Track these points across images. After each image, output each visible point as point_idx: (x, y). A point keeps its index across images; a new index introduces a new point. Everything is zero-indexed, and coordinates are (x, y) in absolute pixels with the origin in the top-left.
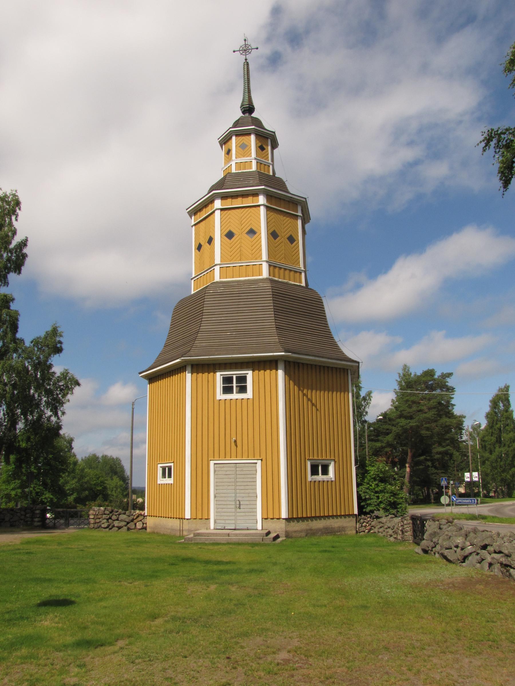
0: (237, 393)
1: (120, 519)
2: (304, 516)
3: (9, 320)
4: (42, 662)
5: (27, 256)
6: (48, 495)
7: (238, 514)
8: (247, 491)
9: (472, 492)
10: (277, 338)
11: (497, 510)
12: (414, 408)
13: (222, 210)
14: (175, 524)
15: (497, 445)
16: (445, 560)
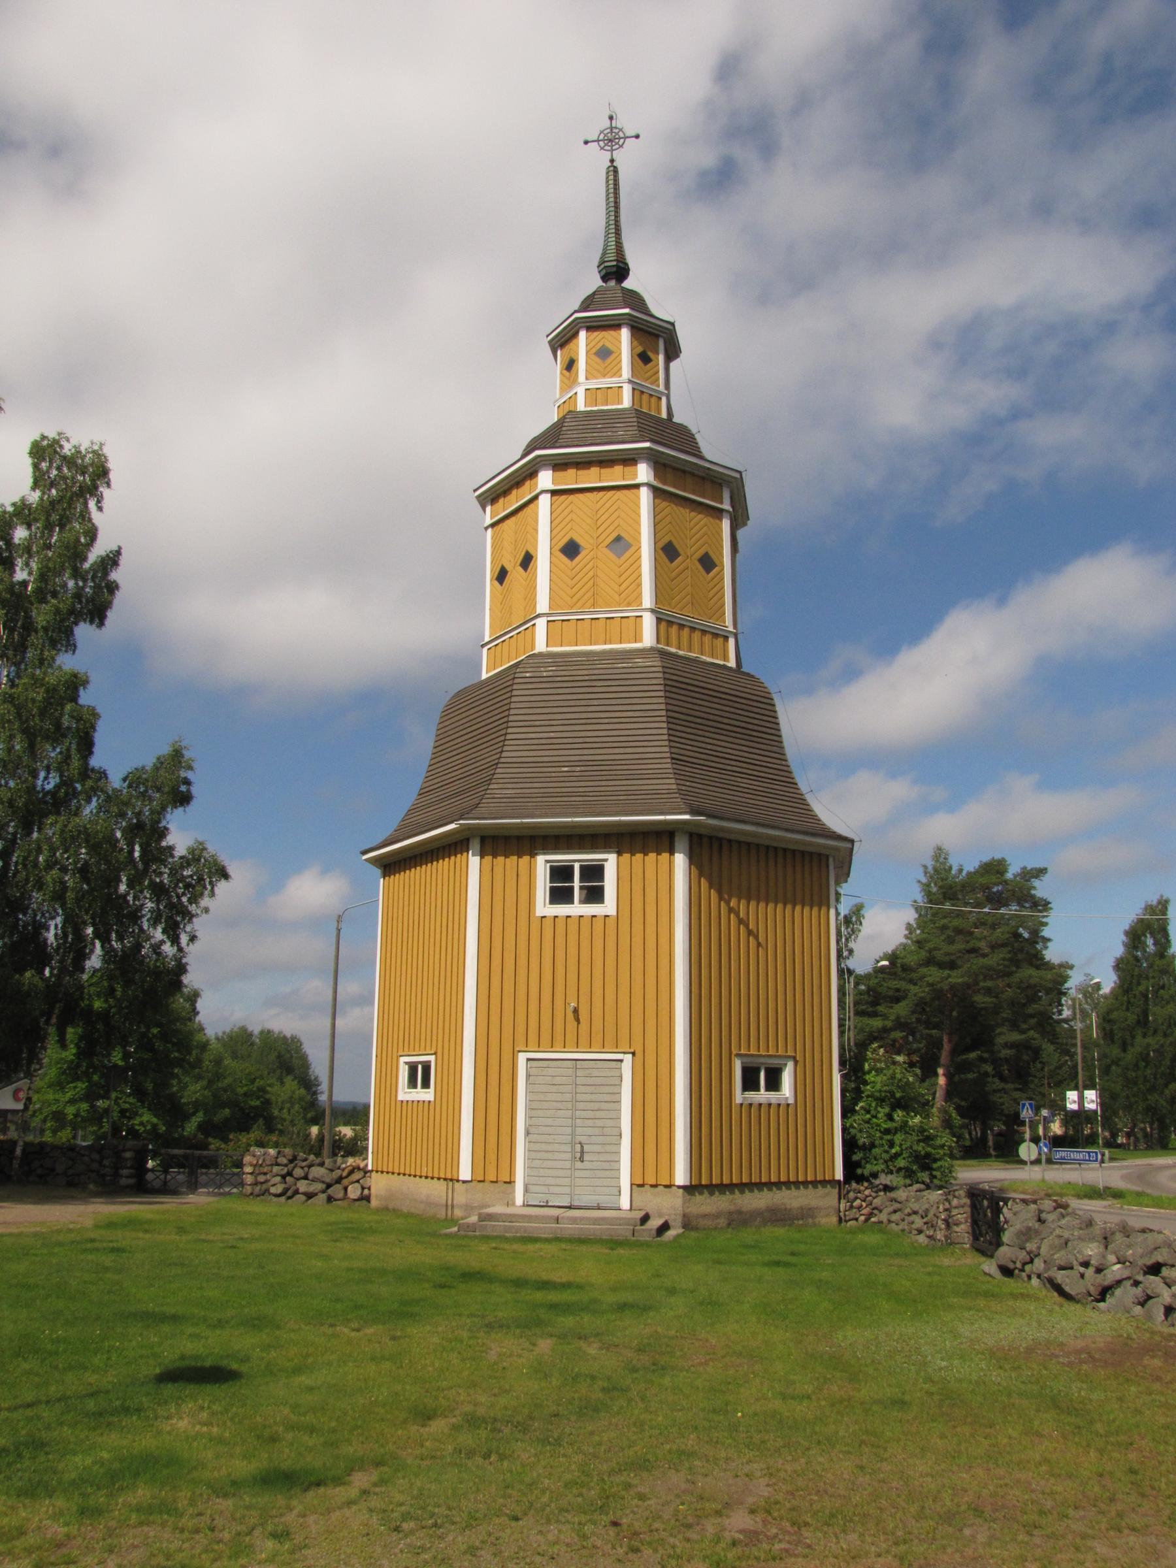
0: (582, 902)
1: (310, 1177)
2: (726, 1181)
3: (78, 729)
4: (187, 1522)
5: (117, 587)
6: (146, 1118)
7: (578, 1174)
8: (599, 1123)
9: (1077, 1134)
10: (673, 781)
11: (1141, 1177)
12: (960, 945)
13: (554, 493)
14: (436, 1190)
15: (1139, 1032)
16: (1055, 1294)
